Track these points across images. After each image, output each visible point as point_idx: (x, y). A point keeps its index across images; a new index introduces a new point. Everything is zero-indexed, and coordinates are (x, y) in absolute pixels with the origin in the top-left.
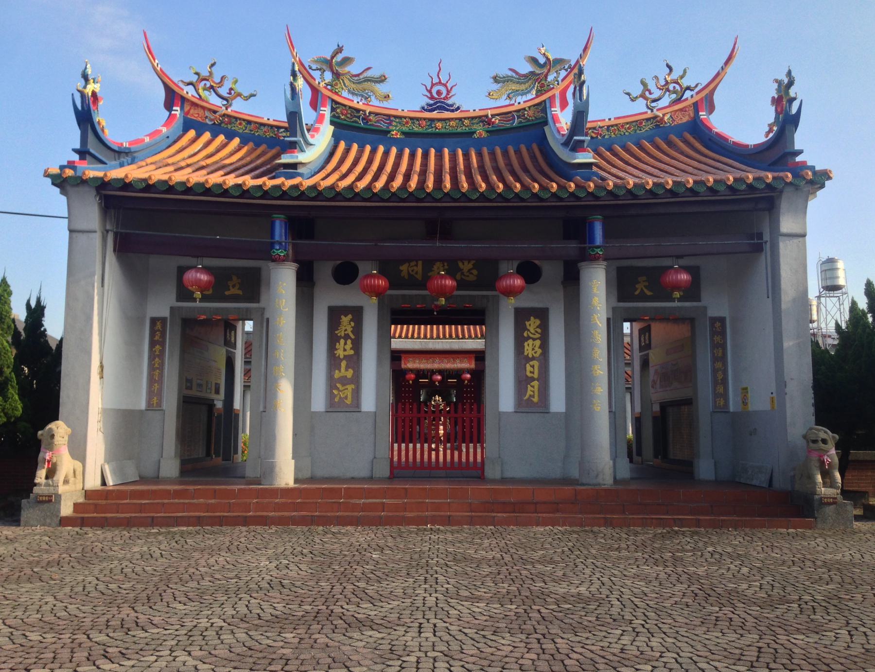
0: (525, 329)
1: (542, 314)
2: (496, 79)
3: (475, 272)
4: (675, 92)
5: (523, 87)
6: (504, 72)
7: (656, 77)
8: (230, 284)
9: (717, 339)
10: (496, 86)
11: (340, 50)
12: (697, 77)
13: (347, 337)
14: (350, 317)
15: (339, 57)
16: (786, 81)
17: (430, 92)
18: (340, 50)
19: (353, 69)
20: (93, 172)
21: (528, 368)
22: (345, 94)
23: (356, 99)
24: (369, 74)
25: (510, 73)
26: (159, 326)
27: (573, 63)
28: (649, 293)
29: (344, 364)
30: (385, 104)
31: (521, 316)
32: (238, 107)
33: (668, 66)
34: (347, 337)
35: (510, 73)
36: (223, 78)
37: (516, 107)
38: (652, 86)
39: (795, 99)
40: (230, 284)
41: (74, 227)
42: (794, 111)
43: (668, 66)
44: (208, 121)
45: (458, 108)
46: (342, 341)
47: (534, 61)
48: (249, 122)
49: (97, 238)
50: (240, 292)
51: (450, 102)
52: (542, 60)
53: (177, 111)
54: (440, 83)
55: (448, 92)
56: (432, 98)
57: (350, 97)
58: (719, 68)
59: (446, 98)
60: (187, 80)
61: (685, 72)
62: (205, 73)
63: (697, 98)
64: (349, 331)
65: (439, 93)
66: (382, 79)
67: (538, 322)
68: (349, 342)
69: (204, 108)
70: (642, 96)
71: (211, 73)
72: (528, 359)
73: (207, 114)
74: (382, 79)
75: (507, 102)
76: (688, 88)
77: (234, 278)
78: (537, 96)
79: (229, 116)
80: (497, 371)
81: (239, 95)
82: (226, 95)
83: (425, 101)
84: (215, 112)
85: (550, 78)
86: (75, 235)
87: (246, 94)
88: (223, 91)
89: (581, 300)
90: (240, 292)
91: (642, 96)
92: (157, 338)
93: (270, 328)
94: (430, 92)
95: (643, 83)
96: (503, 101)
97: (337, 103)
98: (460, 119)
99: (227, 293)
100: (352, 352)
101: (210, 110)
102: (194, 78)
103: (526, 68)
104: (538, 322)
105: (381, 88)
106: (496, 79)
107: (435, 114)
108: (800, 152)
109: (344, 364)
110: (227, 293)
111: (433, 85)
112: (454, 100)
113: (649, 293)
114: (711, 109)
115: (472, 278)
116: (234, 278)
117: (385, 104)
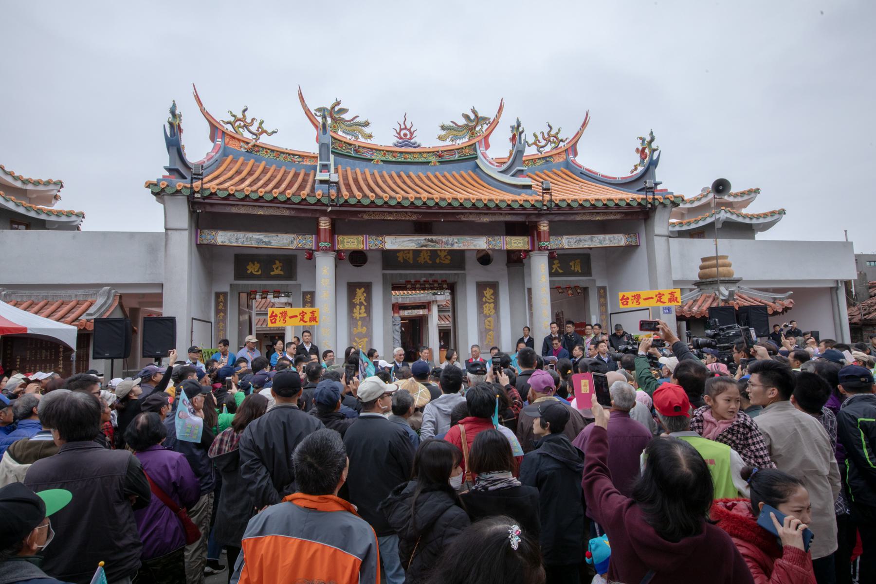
0: (484, 296)
1: (494, 286)
2: (443, 128)
3: (449, 257)
4: (554, 142)
5: (461, 133)
6: (448, 123)
7: (543, 133)
8: (274, 266)
9: (602, 300)
10: (443, 133)
11: (338, 103)
12: (567, 134)
13: (361, 304)
14: (363, 289)
15: (336, 109)
16: (648, 139)
17: (399, 134)
18: (338, 103)
19: (347, 117)
20: (180, 184)
21: (487, 323)
22: (340, 133)
23: (349, 137)
24: (357, 120)
25: (452, 124)
26: (222, 298)
27: (491, 121)
28: (561, 271)
29: (360, 323)
30: (369, 141)
31: (481, 287)
32: (264, 140)
33: (549, 126)
34: (361, 304)
35: (452, 124)
36: (253, 120)
37: (457, 147)
38: (540, 138)
39: (656, 150)
40: (274, 266)
41: (168, 227)
42: (655, 158)
43: (549, 126)
44: (243, 150)
45: (419, 146)
46: (358, 307)
47: (467, 117)
48: (273, 151)
49: (186, 233)
50: (282, 273)
51: (412, 141)
52: (472, 117)
53: (219, 141)
54: (406, 128)
55: (412, 134)
56: (401, 138)
57: (344, 135)
58: (577, 129)
59: (411, 139)
60: (226, 120)
61: (559, 130)
62: (240, 116)
63: (567, 147)
64: (363, 299)
65: (405, 135)
66: (367, 124)
67: (492, 291)
68: (363, 307)
69: (239, 140)
70: (535, 143)
71: (244, 116)
72: (486, 317)
73: (242, 144)
74: (367, 124)
75: (451, 143)
76: (562, 140)
77: (277, 262)
78: (470, 140)
79: (258, 146)
80: (466, 325)
81: (265, 132)
82: (255, 132)
83: (395, 140)
84: (248, 143)
85: (478, 129)
86: (170, 232)
87: (270, 131)
88: (254, 128)
89: (533, 275)
90: (282, 273)
91: (535, 143)
92: (220, 307)
93: (534, 311)
94: (399, 134)
95: (535, 135)
96: (448, 142)
97: (335, 139)
98: (420, 153)
99: (272, 273)
100: (365, 315)
101: (244, 142)
102: (232, 119)
103: (462, 122)
104: (492, 291)
105: (367, 130)
106: (443, 128)
107: (403, 149)
108: (660, 183)
109: (360, 323)
110: (272, 273)
111: (401, 130)
112: (417, 139)
113: (561, 271)
114: (576, 154)
115: (447, 262)
116: (277, 262)
117: (369, 141)
